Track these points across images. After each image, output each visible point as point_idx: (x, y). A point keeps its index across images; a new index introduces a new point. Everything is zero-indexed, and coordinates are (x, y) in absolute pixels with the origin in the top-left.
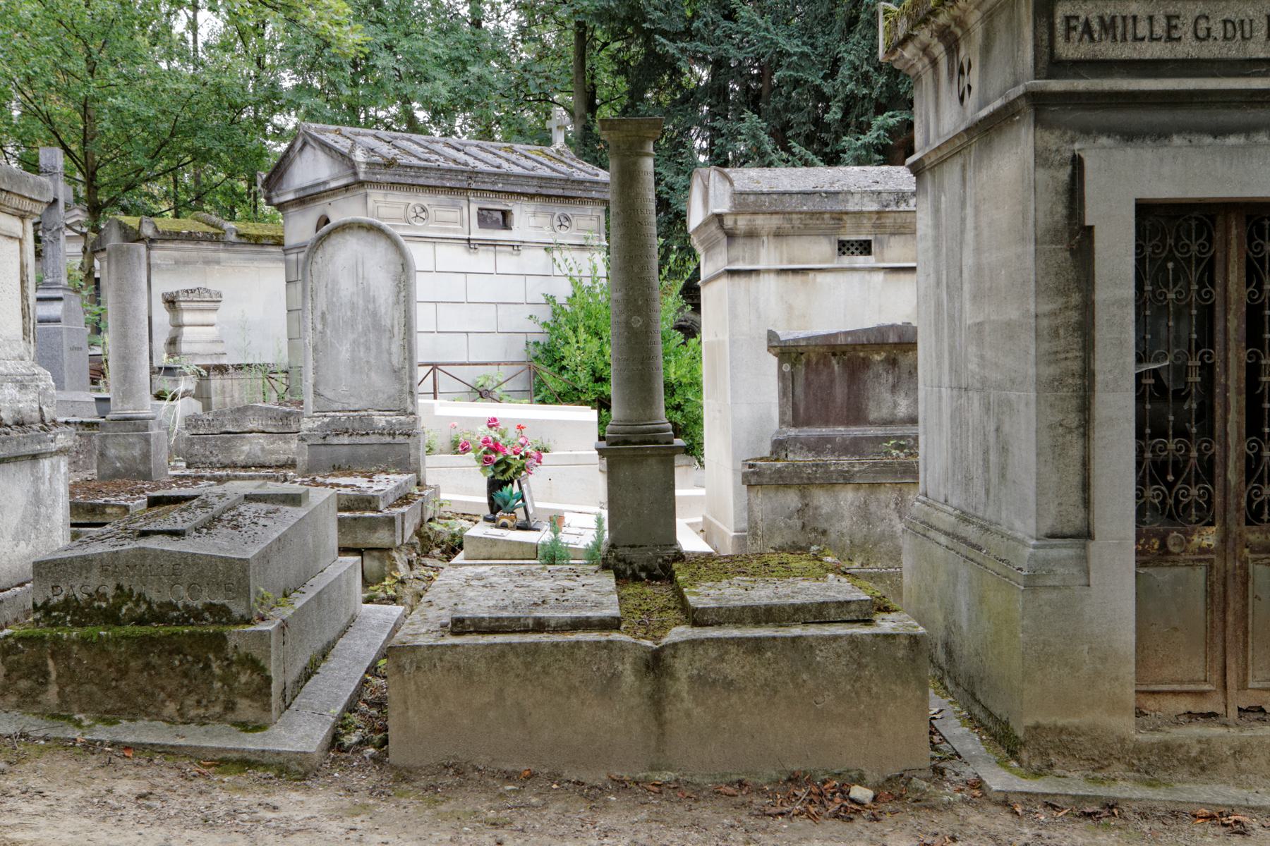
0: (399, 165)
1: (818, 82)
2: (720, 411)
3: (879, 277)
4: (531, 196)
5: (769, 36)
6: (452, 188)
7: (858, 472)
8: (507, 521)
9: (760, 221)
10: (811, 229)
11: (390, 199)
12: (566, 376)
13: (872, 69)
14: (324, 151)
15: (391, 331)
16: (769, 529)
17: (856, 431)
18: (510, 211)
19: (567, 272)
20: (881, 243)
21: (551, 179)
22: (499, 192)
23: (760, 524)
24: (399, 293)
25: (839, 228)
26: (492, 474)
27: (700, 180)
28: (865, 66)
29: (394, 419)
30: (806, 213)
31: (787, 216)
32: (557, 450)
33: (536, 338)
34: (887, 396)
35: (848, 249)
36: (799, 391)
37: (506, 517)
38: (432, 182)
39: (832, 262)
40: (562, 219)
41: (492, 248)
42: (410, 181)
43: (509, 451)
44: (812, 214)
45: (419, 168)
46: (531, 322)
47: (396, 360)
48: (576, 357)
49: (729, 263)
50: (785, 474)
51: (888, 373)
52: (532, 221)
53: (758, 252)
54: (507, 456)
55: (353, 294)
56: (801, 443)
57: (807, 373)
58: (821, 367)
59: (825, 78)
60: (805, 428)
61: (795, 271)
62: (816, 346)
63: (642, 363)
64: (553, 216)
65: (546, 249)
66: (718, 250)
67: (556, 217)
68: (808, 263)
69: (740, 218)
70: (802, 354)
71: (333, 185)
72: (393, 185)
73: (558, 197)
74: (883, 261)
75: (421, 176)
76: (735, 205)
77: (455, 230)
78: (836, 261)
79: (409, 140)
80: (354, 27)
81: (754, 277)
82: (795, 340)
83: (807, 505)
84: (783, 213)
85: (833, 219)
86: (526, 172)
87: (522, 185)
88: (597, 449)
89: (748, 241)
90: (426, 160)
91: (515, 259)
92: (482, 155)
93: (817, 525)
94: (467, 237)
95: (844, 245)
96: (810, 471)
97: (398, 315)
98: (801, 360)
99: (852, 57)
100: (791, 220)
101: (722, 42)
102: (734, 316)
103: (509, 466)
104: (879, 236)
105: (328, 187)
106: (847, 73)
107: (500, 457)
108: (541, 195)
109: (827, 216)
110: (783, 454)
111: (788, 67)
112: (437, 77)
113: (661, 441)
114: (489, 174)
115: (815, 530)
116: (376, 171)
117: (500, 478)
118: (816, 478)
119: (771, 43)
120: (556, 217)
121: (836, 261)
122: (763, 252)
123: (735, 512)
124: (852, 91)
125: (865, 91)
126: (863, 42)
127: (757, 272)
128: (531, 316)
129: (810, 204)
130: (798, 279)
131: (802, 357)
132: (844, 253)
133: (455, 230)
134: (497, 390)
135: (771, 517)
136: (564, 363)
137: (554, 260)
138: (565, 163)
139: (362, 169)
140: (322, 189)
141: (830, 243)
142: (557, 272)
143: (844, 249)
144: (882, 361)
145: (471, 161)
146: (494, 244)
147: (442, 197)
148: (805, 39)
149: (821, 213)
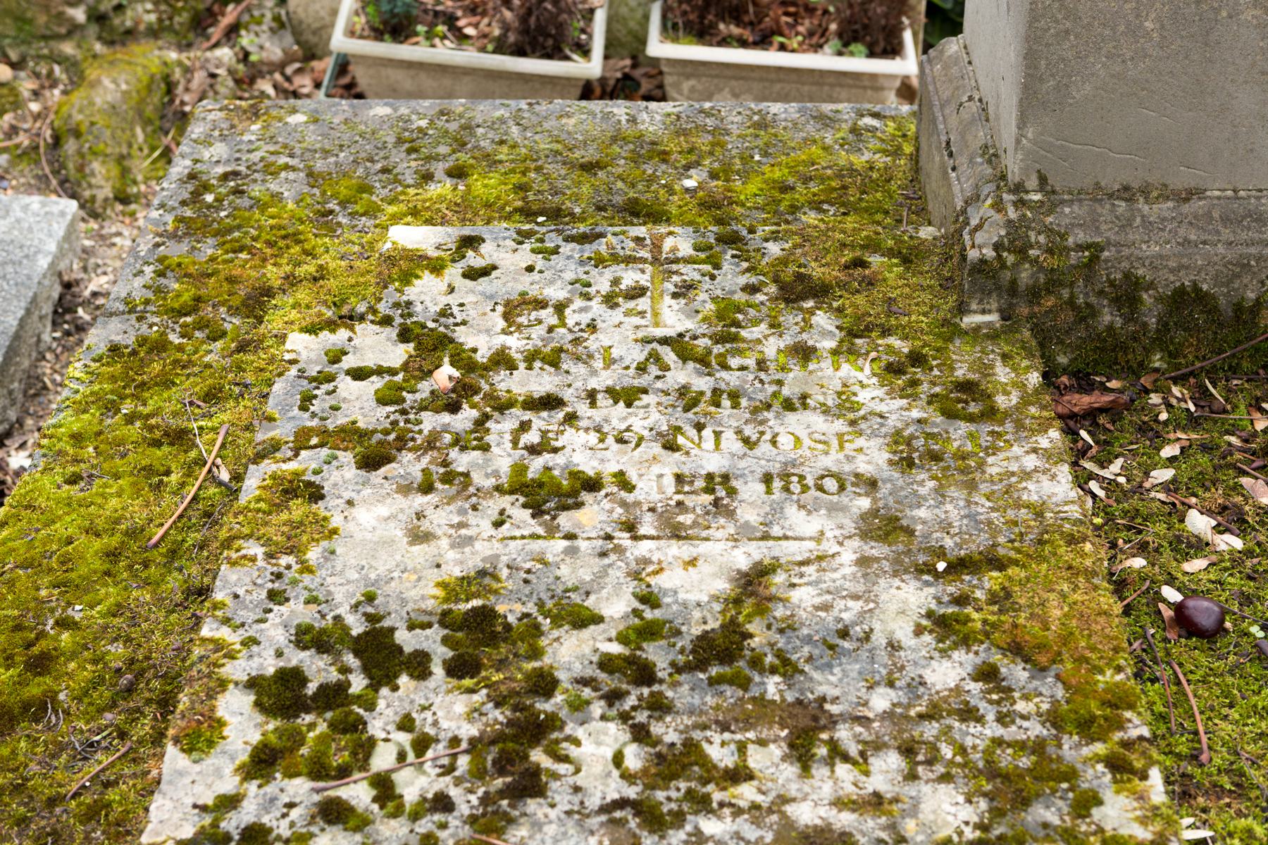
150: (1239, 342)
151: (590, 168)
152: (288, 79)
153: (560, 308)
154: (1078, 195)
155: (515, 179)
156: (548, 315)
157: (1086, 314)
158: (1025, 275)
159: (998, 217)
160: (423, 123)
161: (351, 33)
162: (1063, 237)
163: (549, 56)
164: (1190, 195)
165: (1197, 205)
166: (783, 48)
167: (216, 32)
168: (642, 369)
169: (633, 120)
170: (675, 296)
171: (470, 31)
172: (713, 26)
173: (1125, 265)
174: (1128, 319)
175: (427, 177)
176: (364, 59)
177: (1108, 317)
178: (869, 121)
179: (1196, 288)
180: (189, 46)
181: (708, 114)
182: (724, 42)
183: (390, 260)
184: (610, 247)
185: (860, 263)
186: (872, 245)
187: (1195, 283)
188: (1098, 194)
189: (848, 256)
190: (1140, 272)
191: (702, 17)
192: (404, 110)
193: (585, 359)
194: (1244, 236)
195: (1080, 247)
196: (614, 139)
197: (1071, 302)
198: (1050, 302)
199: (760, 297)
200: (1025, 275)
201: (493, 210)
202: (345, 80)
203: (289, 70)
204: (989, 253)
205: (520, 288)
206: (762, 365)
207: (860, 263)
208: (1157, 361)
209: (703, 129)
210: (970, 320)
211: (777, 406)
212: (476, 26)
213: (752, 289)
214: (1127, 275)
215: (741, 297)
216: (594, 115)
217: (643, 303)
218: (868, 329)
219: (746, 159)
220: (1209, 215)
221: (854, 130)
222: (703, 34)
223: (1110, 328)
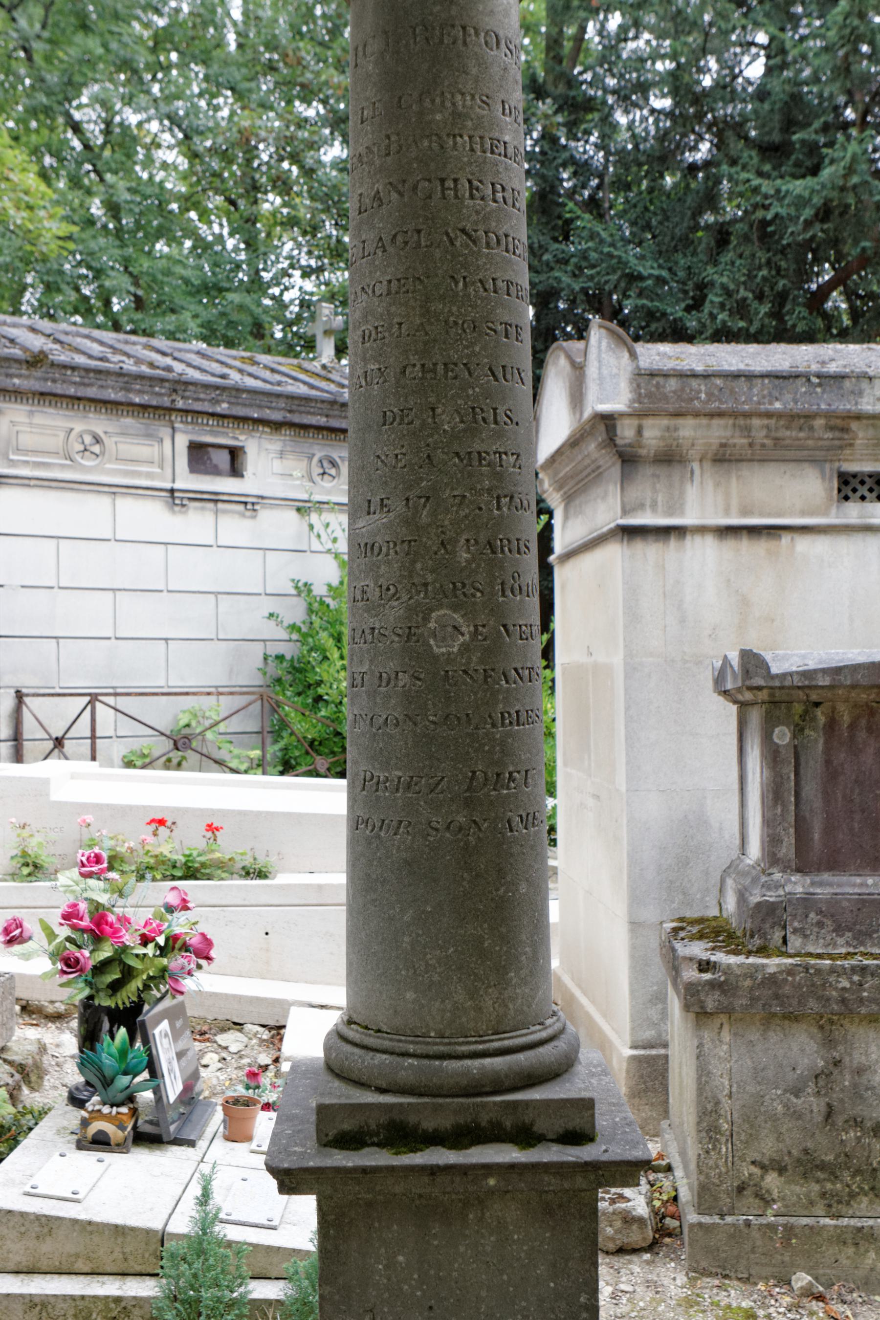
0: (53, 364)
1: (680, 314)
2: (597, 797)
4: (276, 426)
5: (616, 253)
6: (144, 407)
8: (109, 1128)
10: (787, 448)
11: (39, 419)
12: (323, 713)
13: (750, 295)
16: (746, 1118)
18: (242, 448)
19: (329, 545)
21: (307, 399)
22: (223, 416)
23: (726, 1104)
25: (841, 448)
26: (87, 992)
27: (563, 361)
28: (742, 291)
30: (779, 415)
31: (741, 422)
32: (284, 871)
33: (274, 649)
35: (854, 490)
36: (811, 789)
37: (108, 1118)
38: (112, 395)
39: (826, 514)
40: (326, 464)
41: (211, 505)
42: (72, 391)
43: (130, 939)
44: (791, 418)
45: (88, 370)
46: (272, 623)
48: (339, 681)
49: (625, 512)
50: (787, 990)
52: (278, 466)
53: (682, 493)
54: (125, 949)
56: (820, 912)
57: (827, 750)
58: (862, 735)
59: (688, 309)
60: (826, 876)
61: (754, 531)
62: (853, 687)
63: (468, 803)
64: (310, 458)
65: (299, 510)
67: (315, 460)
68: (779, 515)
69: (648, 422)
70: (817, 704)
72: (44, 397)
73: (319, 428)
75: (90, 385)
76: (639, 398)
77: (149, 475)
78: (834, 510)
79: (87, 337)
80: (52, 211)
81: (673, 542)
82: (807, 674)
83: (837, 1063)
84: (734, 414)
85: (832, 428)
86: (268, 387)
87: (260, 407)
88: (273, 1170)
89: (662, 470)
90: (101, 359)
91: (247, 523)
92: (205, 363)
93: (859, 1110)
94: (168, 485)
95: (846, 483)
96: (845, 984)
98: (814, 719)
99: (725, 280)
100: (748, 429)
101: (552, 269)
102: (633, 616)
103: (128, 973)
106: (717, 300)
107: (106, 952)
108: (292, 425)
109: (819, 422)
110: (777, 935)
111: (640, 295)
112: (186, 306)
113: (541, 1126)
114: (206, 386)
115: (856, 1122)
116: (12, 371)
117: (105, 1001)
118: (861, 1000)
119: (619, 263)
120: (315, 460)
121: (834, 510)
122: (692, 492)
123: (632, 1007)
124: (724, 322)
125: (742, 324)
126: (738, 262)
127: (680, 531)
128: (271, 615)
129: (788, 397)
130: (761, 547)
131: (819, 712)
132: (846, 498)
133: (149, 475)
134: (209, 735)
135: (751, 1089)
136: (321, 691)
137: (311, 527)
138: (333, 382)
141: (823, 478)
142: (316, 546)
145: (178, 367)
146: (214, 499)
147: (128, 421)
148: (661, 261)
149: (809, 417)
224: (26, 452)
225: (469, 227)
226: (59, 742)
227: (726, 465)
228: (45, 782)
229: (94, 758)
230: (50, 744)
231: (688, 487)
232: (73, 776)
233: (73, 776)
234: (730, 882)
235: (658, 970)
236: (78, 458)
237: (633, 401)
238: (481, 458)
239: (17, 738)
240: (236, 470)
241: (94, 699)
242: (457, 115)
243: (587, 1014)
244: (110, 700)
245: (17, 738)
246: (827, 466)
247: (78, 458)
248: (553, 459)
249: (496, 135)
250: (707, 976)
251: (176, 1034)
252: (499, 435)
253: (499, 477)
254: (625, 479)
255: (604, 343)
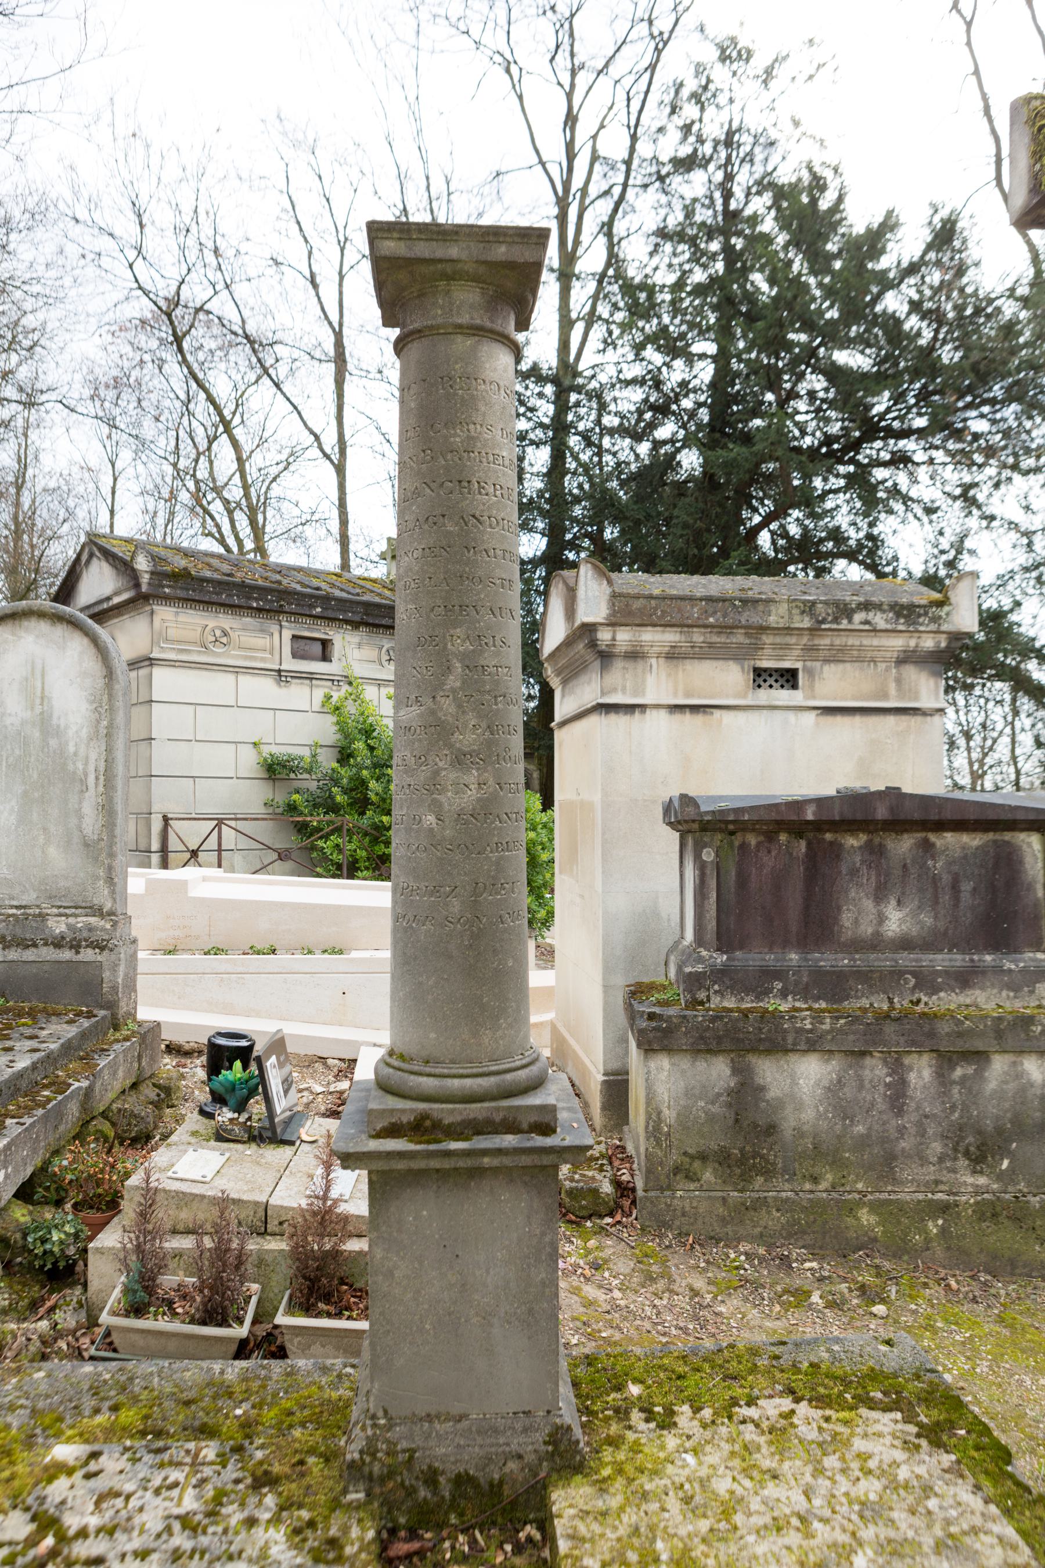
2: (582, 897)
3: (811, 717)
7: (828, 1032)
9: (649, 636)
11: (182, 618)
14: (107, 561)
15: (83, 782)
17: (827, 960)
20: (810, 673)
23: (666, 1112)
24: (98, 722)
27: (561, 585)
29: (81, 922)
30: (712, 626)
34: (868, 904)
39: (745, 697)
42: (207, 598)
47: (91, 822)
49: (603, 694)
51: (869, 867)
53: (644, 681)
55: (23, 723)
61: (695, 709)
64: (381, 649)
66: (583, 678)
67: (384, 650)
68: (711, 697)
71: (116, 600)
74: (814, 698)
76: (613, 613)
77: (263, 660)
78: (750, 695)
82: (737, 811)
89: (630, 664)
94: (277, 667)
95: (759, 675)
97: (95, 755)
104: (809, 664)
105: (111, 603)
108: (367, 624)
120: (384, 650)
121: (750, 695)
122: (651, 680)
123: (605, 1046)
127: (642, 708)
130: (699, 719)
132: (759, 686)
133: (263, 660)
139: (145, 579)
140: (105, 606)
143: (760, 681)
144: (860, 848)
150: (494, 1506)
151: (187, 1403)
152: (77, 1340)
153: (128, 1497)
154: (404, 1420)
155: (144, 1411)
156: (119, 1502)
157: (411, 1492)
158: (376, 1469)
159: (362, 1434)
160: (108, 1376)
161: (114, 1313)
162: (395, 1445)
163: (220, 1325)
164: (460, 1418)
165: (465, 1424)
166: (349, 1318)
167: (42, 1311)
168: (159, 1536)
169: (222, 1372)
170: (195, 1487)
171: (180, 1310)
172: (315, 1305)
173: (427, 1461)
174: (435, 1493)
175: (97, 1411)
176: (118, 1328)
177: (423, 1493)
178: (349, 1370)
179: (467, 1474)
180: (25, 1319)
181: (263, 1367)
182: (318, 1315)
183: (46, 1468)
184: (171, 1456)
185: (302, 1462)
186: (312, 1451)
187: (466, 1471)
188: (415, 1419)
189: (297, 1457)
190: (436, 1465)
191: (308, 1300)
192: (100, 1369)
193: (128, 1530)
194: (488, 1441)
195: (404, 1451)
196: (208, 1385)
197: (402, 1483)
198: (391, 1485)
199: (241, 1486)
200: (376, 1469)
201: (110, 1433)
202: (108, 1340)
203: (79, 1333)
204: (356, 1456)
205: (111, 1484)
206: (225, 1531)
207: (302, 1462)
208: (453, 1519)
209: (258, 1377)
210: (352, 1497)
211: (224, 1559)
212: (183, 1307)
213: (237, 1481)
214: (430, 1467)
215: (229, 1487)
216: (202, 1369)
217: (175, 1492)
218: (291, 1505)
219: (275, 1395)
220: (470, 1429)
221: (339, 1376)
222: (308, 1310)
223: (425, 1499)
224: (173, 641)
225: (477, 514)
226: (194, 853)
227: (675, 661)
228: (183, 884)
229: (220, 866)
230: (188, 855)
231: (648, 675)
232: (205, 879)
233: (205, 879)
234: (672, 958)
235: (622, 1019)
236: (211, 646)
237: (610, 615)
238: (484, 670)
239: (164, 850)
240: (325, 657)
241: (220, 822)
242: (470, 438)
243: (574, 1051)
244: (232, 823)
245: (164, 850)
246: (746, 663)
247: (211, 646)
248: (553, 655)
249: (497, 452)
250: (654, 1024)
251: (281, 1065)
252: (497, 654)
253: (497, 683)
254: (604, 668)
255: (590, 573)
